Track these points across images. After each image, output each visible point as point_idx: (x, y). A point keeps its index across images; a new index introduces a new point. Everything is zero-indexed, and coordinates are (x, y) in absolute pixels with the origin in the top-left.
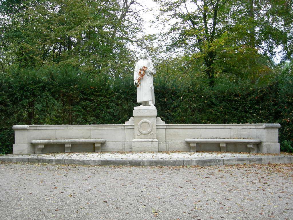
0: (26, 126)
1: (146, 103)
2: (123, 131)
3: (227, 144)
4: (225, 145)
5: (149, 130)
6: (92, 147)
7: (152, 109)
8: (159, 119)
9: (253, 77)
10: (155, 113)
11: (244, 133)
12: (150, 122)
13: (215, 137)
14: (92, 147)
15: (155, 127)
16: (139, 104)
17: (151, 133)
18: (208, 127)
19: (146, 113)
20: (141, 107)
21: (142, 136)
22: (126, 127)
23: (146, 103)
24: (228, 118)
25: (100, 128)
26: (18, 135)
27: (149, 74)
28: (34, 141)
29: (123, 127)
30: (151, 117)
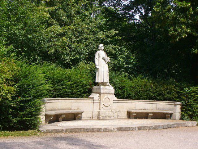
1: (104, 84)
6: (75, 117)
7: (111, 89)
11: (161, 107)
14: (75, 117)
19: (108, 92)
21: (105, 108)
22: (94, 101)
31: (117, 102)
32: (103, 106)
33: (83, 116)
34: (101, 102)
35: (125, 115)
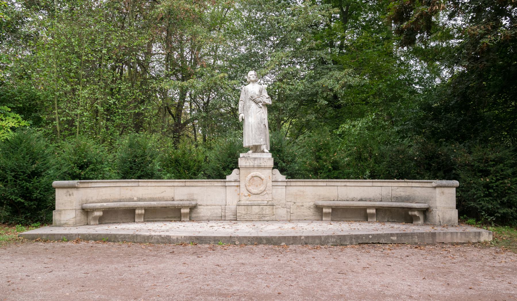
1: (256, 149)
2: (222, 190)
3: (378, 209)
4: (373, 211)
5: (262, 188)
6: (173, 213)
7: (267, 158)
8: (277, 171)
10: (271, 163)
12: (263, 176)
13: (359, 198)
15: (270, 184)
17: (265, 193)
22: (227, 184)
23: (256, 149)
27: (261, 106)
28: (85, 205)
29: (223, 184)
30: (265, 168)
31: (285, 184)
32: (246, 193)
33: (202, 211)
34: (242, 185)
35: (310, 213)
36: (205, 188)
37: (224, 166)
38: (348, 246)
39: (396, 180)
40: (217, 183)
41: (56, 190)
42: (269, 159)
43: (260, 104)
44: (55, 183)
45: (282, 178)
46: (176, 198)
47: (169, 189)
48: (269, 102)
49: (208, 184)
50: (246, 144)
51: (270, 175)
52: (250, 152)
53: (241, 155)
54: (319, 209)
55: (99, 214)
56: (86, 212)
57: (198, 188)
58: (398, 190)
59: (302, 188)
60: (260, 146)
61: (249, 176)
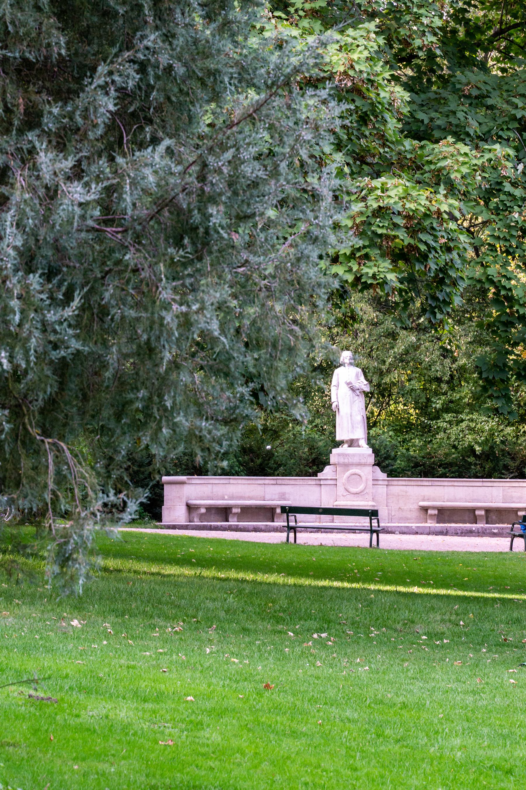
0: (183, 478)
1: (352, 443)
2: (317, 489)
3: (488, 511)
4: (483, 513)
5: (361, 487)
7: (365, 451)
9: (487, 232)
10: (372, 460)
12: (362, 474)
15: (370, 483)
16: (338, 444)
18: (456, 484)
19: (356, 460)
20: (344, 449)
22: (322, 482)
23: (352, 443)
24: (81, 439)
25: (279, 482)
26: (169, 492)
28: (190, 502)
29: (318, 482)
30: (365, 465)
31: (386, 483)
36: (298, 487)
37: (313, 463)
38: (251, 110)
39: (196, 477)
40: (310, 481)
41: (166, 487)
42: (369, 455)
43: (358, 392)
44: (165, 478)
45: (384, 476)
46: (267, 497)
47: (260, 488)
48: (367, 389)
49: (301, 482)
50: (338, 438)
51: (370, 473)
52: (346, 446)
53: (334, 451)
54: (425, 509)
55: (203, 511)
56: (190, 508)
57: (290, 486)
58: (510, 491)
59: (404, 488)
60: (358, 440)
61: (348, 474)
